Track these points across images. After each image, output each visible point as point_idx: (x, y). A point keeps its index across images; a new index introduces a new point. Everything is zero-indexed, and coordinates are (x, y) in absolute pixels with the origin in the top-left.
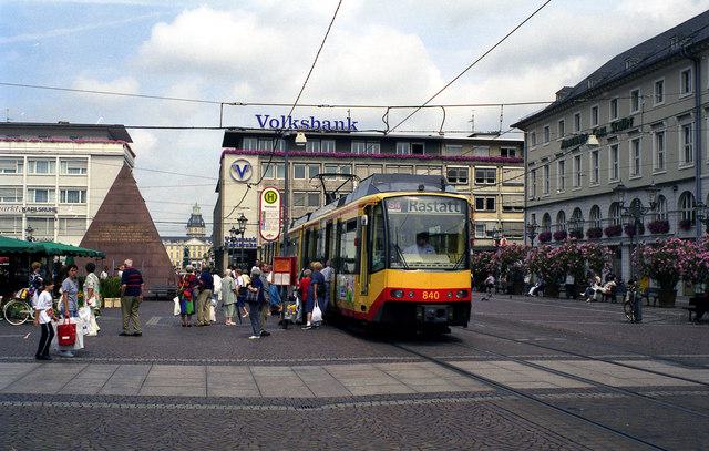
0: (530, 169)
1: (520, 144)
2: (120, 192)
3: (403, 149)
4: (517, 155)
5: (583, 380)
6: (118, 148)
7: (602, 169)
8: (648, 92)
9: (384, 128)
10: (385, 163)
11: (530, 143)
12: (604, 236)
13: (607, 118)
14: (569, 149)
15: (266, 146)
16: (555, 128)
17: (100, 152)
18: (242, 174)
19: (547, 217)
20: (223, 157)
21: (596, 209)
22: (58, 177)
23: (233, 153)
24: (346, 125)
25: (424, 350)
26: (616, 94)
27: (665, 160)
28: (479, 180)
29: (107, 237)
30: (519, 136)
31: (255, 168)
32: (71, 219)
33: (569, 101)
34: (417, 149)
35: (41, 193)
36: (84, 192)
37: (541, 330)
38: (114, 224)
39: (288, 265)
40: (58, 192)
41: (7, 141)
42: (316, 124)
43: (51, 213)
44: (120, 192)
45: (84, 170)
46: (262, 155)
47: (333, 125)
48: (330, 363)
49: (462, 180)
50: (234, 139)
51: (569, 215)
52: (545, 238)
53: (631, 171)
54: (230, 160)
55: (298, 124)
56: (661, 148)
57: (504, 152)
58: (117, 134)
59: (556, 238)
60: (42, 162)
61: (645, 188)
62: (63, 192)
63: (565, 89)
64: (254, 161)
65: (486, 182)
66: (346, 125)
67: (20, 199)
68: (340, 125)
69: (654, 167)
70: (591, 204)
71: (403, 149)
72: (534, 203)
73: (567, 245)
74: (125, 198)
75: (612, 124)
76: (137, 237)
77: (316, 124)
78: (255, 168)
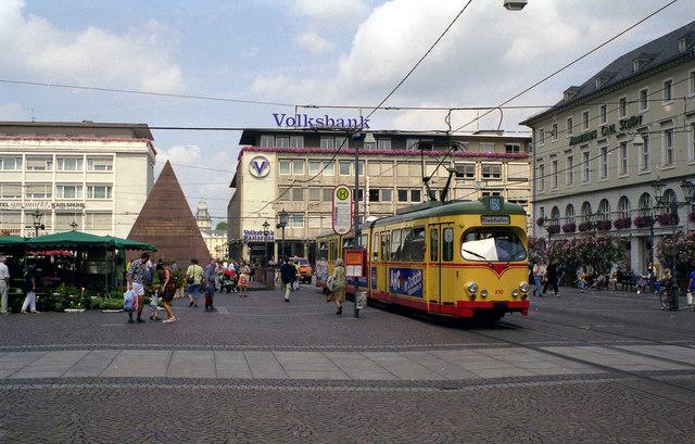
0: (538, 165)
1: (528, 141)
2: (163, 188)
3: (411, 145)
4: (521, 152)
5: (628, 352)
6: (141, 146)
7: (614, 170)
8: (655, 89)
10: (396, 159)
11: (538, 138)
12: (613, 228)
13: (615, 117)
14: (578, 147)
15: (282, 143)
16: (563, 125)
17: (125, 150)
18: (260, 171)
19: (555, 210)
20: (242, 154)
21: (624, 200)
22: (84, 175)
23: (252, 150)
24: (359, 122)
25: (486, 333)
26: (648, 84)
27: (649, 162)
28: (485, 175)
29: (152, 232)
30: (527, 132)
31: (273, 165)
32: (98, 213)
33: (576, 100)
34: (422, 146)
35: (69, 188)
36: (109, 189)
37: (605, 319)
38: (159, 219)
39: (360, 258)
40: (84, 187)
41: (38, 140)
42: (330, 122)
43: (80, 208)
44: (163, 188)
45: (110, 167)
46: (279, 152)
47: (346, 123)
49: (495, 176)
50: (251, 138)
51: (595, 208)
52: (553, 230)
53: (619, 170)
54: (248, 157)
55: (313, 122)
56: (670, 145)
57: (509, 148)
58: (141, 132)
59: (580, 229)
60: (70, 160)
61: (652, 184)
62: (90, 188)
63: (572, 88)
64: (272, 158)
65: (491, 177)
66: (359, 122)
67: (49, 195)
68: (353, 123)
69: (640, 167)
70: (600, 198)
71: (411, 145)
72: (540, 198)
73: (578, 236)
74: (165, 193)
75: (621, 121)
76: (180, 231)
77: (330, 122)
78: (273, 165)
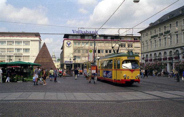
0: (142, 43)
1: (140, 37)
2: (43, 50)
3: (109, 38)
4: (138, 40)
5: (166, 93)
6: (37, 38)
7: (163, 45)
8: (173, 23)
9: (118, 34)
10: (105, 42)
11: (142, 36)
12: (162, 60)
13: (163, 31)
14: (153, 39)
15: (75, 38)
16: (149, 33)
17: (33, 39)
18: (69, 45)
19: (147, 55)
20: (64, 40)
21: (165, 53)
22: (22, 46)
23: (67, 40)
24: (95, 32)
25: (129, 88)
26: (171, 22)
27: (172, 43)
28: (128, 46)
29: (40, 61)
30: (139, 35)
31: (72, 44)
32: (26, 56)
33: (153, 26)
34: (112, 38)
35: (18, 50)
36: (29, 50)
37: (160, 84)
38: (42, 58)
39: (95, 68)
40: (22, 49)
41: (10, 37)
42: (87, 32)
43: (21, 55)
44: (43, 50)
45: (29, 44)
46: (74, 40)
47: (92, 32)
48: (88, 92)
49: (131, 46)
50: (66, 36)
51: (157, 55)
52: (146, 61)
53: (164, 45)
54: (66, 41)
55: (83, 32)
56: (177, 38)
57: (135, 39)
58: (37, 35)
59: (154, 60)
60: (19, 42)
61: (173, 48)
62: (24, 50)
63: (151, 23)
64: (72, 42)
65: (130, 47)
66: (95, 32)
67: (13, 51)
68: (93, 32)
69: (169, 44)
70: (159, 52)
71: (109, 38)
72: (143, 52)
73: (153, 62)
74: (44, 51)
75: (164, 32)
76: (48, 61)
77: (87, 32)
78: (72, 44)
